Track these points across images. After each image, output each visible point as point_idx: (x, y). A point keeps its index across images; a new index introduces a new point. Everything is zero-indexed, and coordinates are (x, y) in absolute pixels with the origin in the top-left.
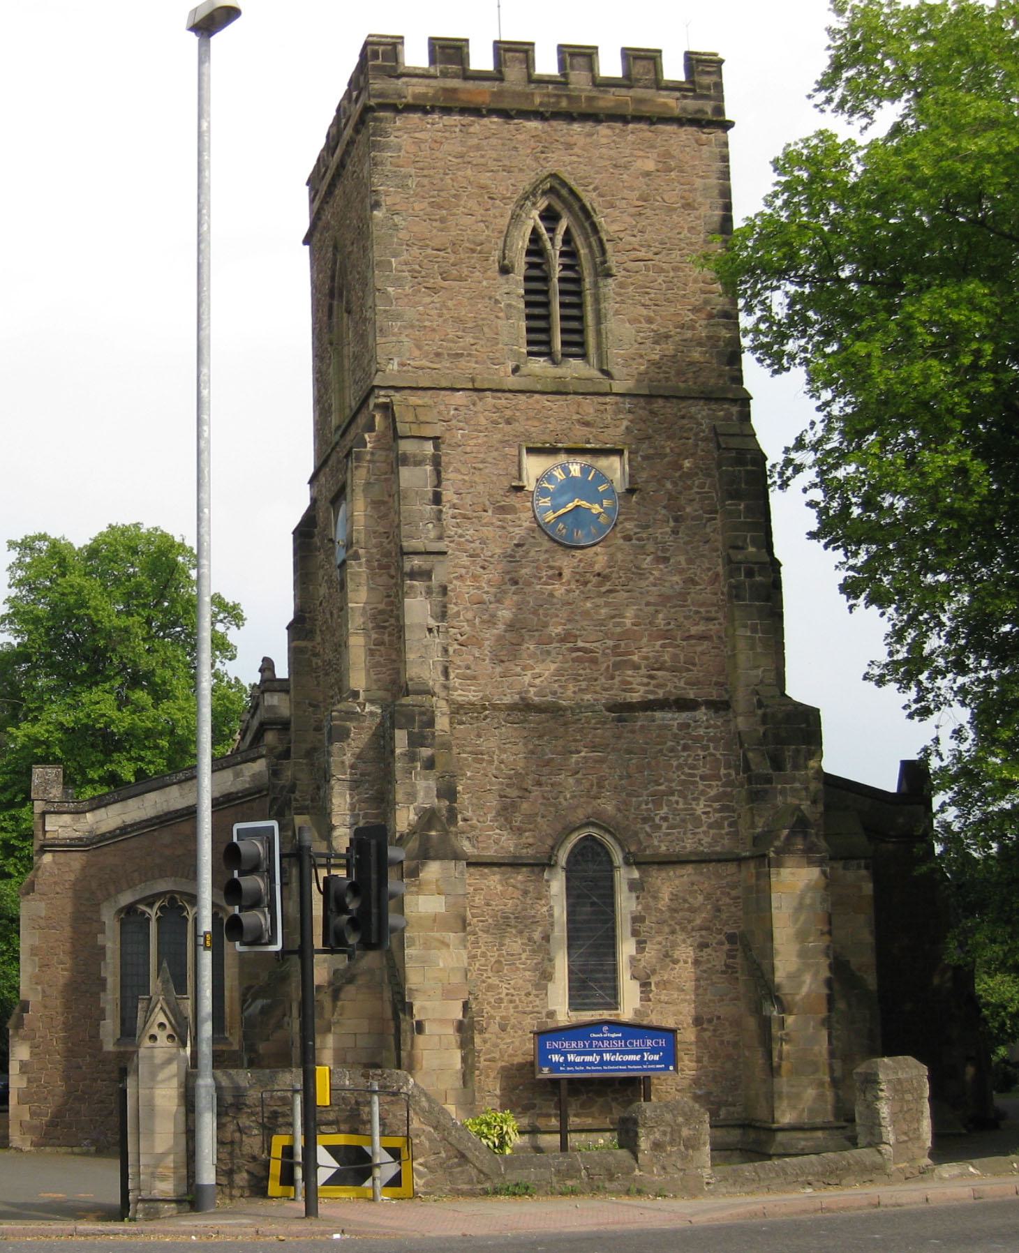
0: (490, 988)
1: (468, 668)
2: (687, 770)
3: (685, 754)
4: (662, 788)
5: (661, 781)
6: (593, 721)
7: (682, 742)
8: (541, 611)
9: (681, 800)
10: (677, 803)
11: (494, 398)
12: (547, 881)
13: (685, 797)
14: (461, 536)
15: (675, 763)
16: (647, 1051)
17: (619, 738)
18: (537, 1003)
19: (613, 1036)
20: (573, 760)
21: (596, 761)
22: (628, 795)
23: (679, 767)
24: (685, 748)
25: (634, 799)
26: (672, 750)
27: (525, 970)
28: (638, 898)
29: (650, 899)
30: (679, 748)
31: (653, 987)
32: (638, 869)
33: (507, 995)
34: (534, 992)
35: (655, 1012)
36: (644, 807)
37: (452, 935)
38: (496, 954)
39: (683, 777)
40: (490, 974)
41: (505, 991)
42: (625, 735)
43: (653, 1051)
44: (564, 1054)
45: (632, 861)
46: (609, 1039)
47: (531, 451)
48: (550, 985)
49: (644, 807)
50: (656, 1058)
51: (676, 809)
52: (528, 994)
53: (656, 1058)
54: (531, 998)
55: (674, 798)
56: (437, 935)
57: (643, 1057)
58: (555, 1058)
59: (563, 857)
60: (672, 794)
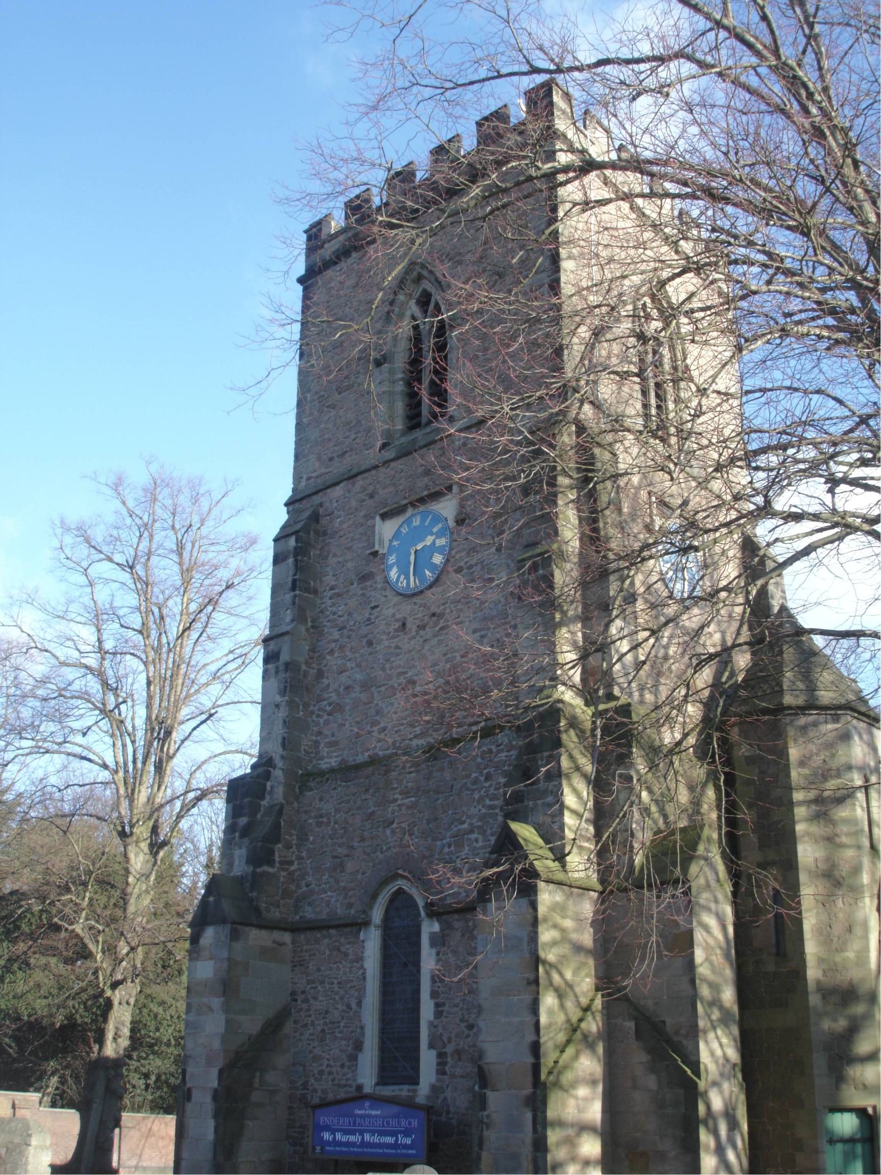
0: (316, 1058)
1: (333, 735)
2: (488, 802)
3: (487, 784)
4: (465, 826)
5: (464, 819)
6: (408, 765)
7: (485, 771)
8: (388, 666)
9: (480, 837)
10: (477, 840)
11: (363, 479)
12: (363, 941)
13: (483, 833)
14: (334, 613)
15: (476, 796)
16: (401, 1132)
17: (429, 779)
18: (350, 1076)
19: (374, 1112)
20: (390, 810)
21: (408, 808)
22: (434, 839)
23: (481, 799)
24: (488, 777)
25: (439, 843)
26: (475, 782)
27: (341, 1039)
28: (438, 954)
29: (450, 955)
30: (482, 779)
31: (449, 1059)
32: (438, 921)
33: (328, 1066)
34: (347, 1064)
35: (450, 1088)
36: (446, 850)
37: (216, 1000)
38: (322, 1022)
39: (484, 811)
40: (316, 1044)
41: (326, 1062)
42: (435, 774)
43: (407, 1134)
44: (333, 1132)
45: (434, 912)
46: (369, 1116)
47: (384, 517)
48: (360, 1056)
49: (446, 850)
50: (408, 1141)
51: (475, 848)
52: (342, 1066)
53: (408, 1141)
54: (346, 1070)
55: (473, 836)
56: (205, 1000)
57: (397, 1140)
58: (327, 1136)
59: (377, 915)
60: (472, 832)
